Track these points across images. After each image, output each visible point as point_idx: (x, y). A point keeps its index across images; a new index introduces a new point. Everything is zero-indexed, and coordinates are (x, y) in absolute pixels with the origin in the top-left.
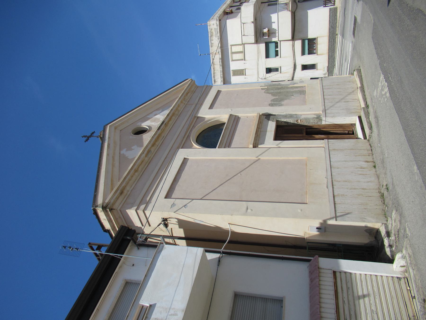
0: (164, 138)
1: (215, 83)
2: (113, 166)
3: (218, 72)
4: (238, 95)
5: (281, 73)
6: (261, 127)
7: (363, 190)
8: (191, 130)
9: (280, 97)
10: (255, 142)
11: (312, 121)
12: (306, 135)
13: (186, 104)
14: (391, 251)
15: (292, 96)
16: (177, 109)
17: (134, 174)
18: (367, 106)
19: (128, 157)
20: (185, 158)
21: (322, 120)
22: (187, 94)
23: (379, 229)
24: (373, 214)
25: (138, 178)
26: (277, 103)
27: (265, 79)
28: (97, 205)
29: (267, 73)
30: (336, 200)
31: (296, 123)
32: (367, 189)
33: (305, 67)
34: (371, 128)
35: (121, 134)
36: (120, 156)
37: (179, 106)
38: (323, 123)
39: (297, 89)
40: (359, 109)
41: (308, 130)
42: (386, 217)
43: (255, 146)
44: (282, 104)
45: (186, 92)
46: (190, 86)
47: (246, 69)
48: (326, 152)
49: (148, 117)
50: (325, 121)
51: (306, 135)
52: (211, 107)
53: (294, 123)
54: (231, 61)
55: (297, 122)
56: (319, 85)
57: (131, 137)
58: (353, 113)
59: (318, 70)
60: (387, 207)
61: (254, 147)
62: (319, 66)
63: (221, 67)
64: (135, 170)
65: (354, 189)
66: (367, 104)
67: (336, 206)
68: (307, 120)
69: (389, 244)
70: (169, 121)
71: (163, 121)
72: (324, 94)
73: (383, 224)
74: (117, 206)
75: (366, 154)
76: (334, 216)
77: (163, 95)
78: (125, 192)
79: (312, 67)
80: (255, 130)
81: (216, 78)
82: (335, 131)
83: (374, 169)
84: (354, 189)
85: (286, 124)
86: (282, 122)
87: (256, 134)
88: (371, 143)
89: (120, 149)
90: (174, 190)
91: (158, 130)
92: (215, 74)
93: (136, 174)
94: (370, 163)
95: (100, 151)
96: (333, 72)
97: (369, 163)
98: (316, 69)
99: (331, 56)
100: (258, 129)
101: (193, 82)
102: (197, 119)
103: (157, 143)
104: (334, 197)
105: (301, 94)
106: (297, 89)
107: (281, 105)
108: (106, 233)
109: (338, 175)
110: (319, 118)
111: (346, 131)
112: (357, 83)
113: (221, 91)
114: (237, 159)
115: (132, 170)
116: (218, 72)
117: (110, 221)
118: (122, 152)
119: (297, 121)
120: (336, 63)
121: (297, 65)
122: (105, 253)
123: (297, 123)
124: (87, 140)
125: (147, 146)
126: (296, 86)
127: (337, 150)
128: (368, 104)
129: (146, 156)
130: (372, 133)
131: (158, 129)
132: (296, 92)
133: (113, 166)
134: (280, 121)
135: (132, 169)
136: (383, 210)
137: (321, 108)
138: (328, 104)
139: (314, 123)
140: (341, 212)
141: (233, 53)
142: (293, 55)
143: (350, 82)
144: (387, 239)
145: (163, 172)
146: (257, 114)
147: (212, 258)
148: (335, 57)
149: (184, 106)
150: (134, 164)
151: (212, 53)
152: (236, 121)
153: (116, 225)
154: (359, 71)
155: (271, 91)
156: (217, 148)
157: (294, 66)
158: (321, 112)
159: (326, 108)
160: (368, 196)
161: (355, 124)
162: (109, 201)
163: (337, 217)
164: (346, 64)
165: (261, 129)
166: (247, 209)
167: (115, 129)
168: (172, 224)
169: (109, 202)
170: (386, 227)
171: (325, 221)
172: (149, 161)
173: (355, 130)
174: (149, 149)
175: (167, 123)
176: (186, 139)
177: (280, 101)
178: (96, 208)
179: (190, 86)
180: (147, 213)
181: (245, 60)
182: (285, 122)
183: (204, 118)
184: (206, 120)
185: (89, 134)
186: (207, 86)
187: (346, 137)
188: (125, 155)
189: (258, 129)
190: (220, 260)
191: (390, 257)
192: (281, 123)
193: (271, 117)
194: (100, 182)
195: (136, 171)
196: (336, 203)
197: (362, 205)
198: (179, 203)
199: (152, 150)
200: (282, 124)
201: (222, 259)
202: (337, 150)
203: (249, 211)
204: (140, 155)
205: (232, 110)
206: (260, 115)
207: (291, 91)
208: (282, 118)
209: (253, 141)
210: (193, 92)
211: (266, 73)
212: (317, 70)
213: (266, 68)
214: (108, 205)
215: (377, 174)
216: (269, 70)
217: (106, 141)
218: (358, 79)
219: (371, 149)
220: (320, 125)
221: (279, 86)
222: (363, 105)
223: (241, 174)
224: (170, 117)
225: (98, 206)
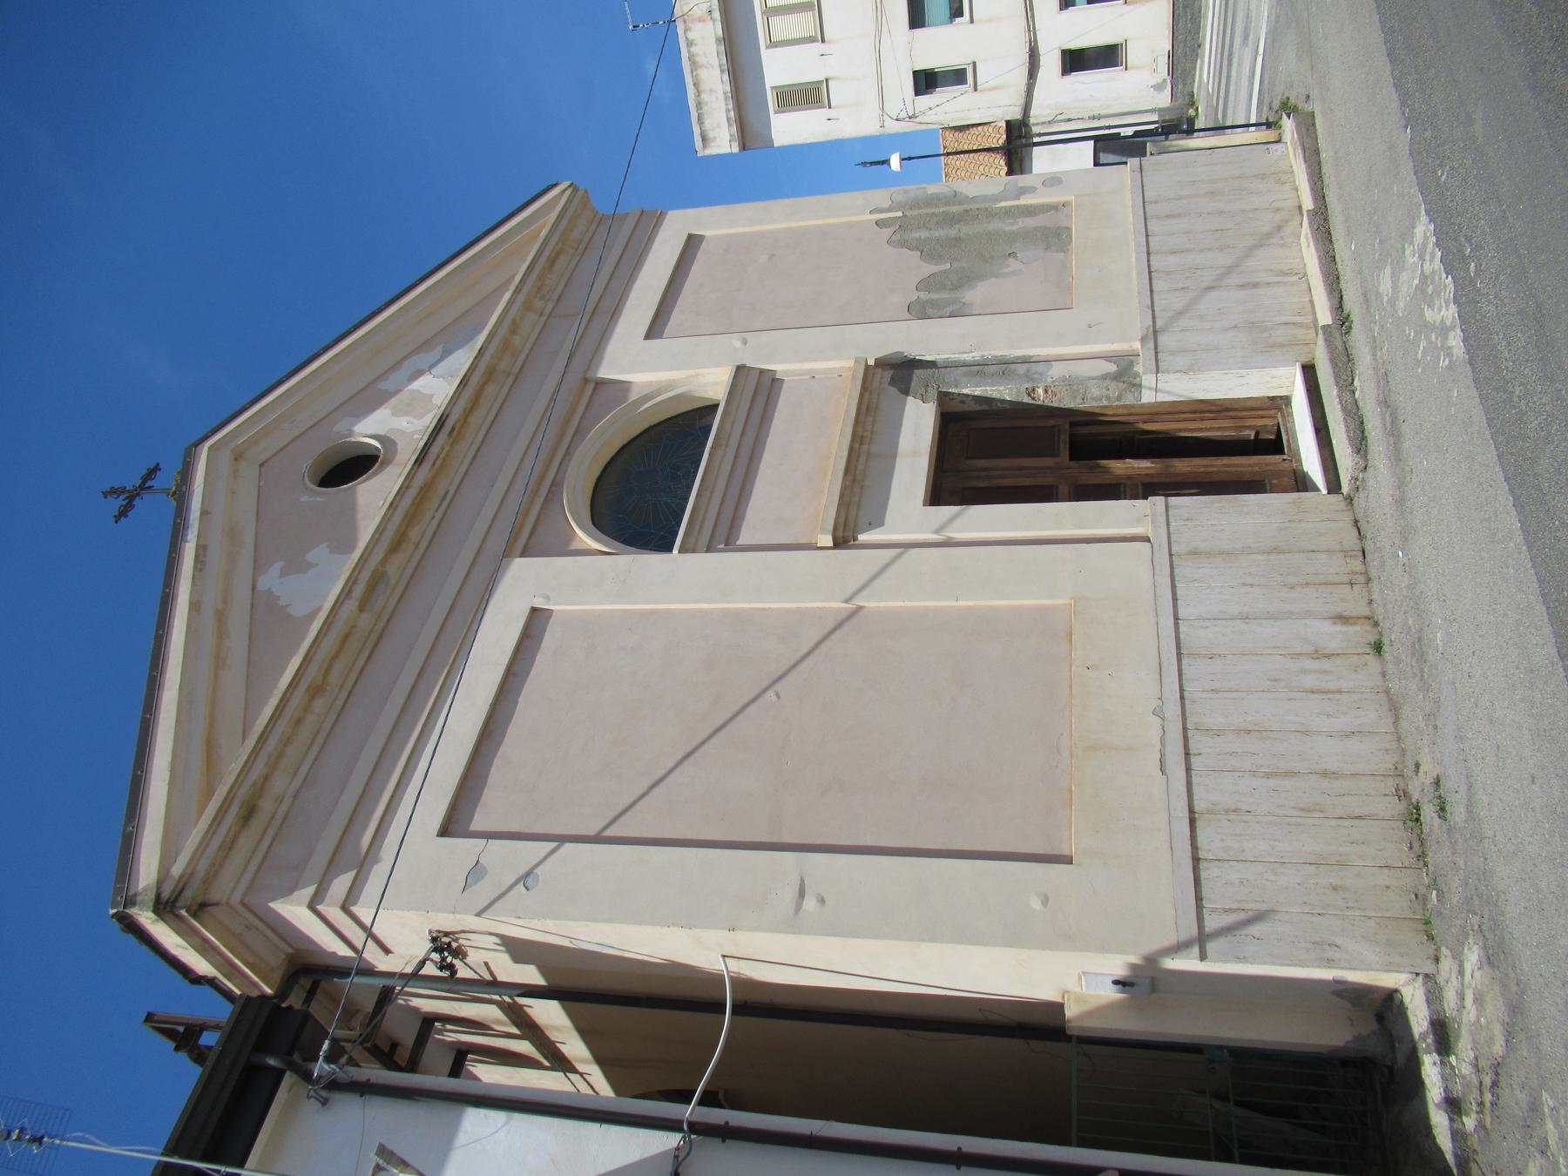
0: (445, 503)
1: (704, 146)
2: (219, 661)
3: (717, 98)
4: (773, 255)
5: (976, 89)
6: (872, 433)
7: (1325, 784)
8: (568, 454)
9: (955, 265)
10: (842, 520)
11: (1095, 391)
12: (1071, 459)
13: (547, 312)
14: (1458, 1135)
15: (1011, 260)
16: (506, 346)
17: (307, 708)
18: (1343, 320)
19: (288, 610)
20: (534, 610)
21: (1140, 386)
22: (552, 261)
23: (1396, 991)
24: (1370, 918)
25: (327, 725)
26: (945, 295)
27: (910, 118)
28: (131, 892)
29: (918, 92)
30: (1202, 839)
31: (1026, 400)
32: (1343, 776)
33: (1075, 61)
34: (1360, 444)
35: (261, 484)
36: (252, 605)
37: (514, 328)
38: (1147, 397)
39: (1031, 222)
40: (1308, 328)
41: (1082, 430)
42: (1431, 938)
43: (843, 537)
44: (964, 303)
45: (547, 253)
46: (564, 223)
47: (830, 83)
48: (1157, 567)
49: (383, 385)
50: (1156, 390)
51: (1071, 459)
52: (655, 330)
53: (1020, 400)
54: (767, 48)
55: (1029, 395)
56: (1128, 200)
57: (305, 499)
58: (1281, 345)
59: (1132, 68)
60: (1438, 892)
61: (841, 541)
62: (1133, 55)
63: (726, 77)
64: (310, 686)
65: (1288, 774)
66: (1341, 307)
67: (1203, 875)
68: (1075, 387)
69: (1445, 1091)
70: (468, 413)
71: (443, 414)
72: (1151, 244)
73: (1417, 974)
74: (226, 889)
75: (1336, 579)
76: (1194, 932)
77: (448, 275)
78: (266, 804)
79: (1107, 56)
80: (845, 454)
81: (708, 123)
82: (1200, 430)
83: (1373, 662)
84: (1288, 774)
85: (985, 407)
86: (965, 398)
87: (847, 471)
88: (1360, 516)
89: (257, 568)
90: (482, 789)
91: (419, 466)
92: (705, 108)
93: (319, 704)
94: (1357, 628)
95: (164, 592)
96: (1194, 75)
97: (1351, 629)
98: (1122, 65)
99: (1185, 7)
100: (857, 446)
101: (580, 194)
102: (595, 389)
103: (414, 534)
104: (1192, 821)
105: (1047, 248)
106: (1031, 222)
107: (959, 312)
108: (201, 987)
109: (1210, 695)
110: (1124, 372)
111: (1247, 432)
112: (1297, 183)
113: (701, 238)
114: (764, 609)
115: (295, 687)
116: (717, 98)
117: (205, 949)
118: (264, 583)
119: (1031, 392)
120: (1204, 36)
121: (1041, 53)
122: (163, 1154)
123: (1033, 402)
124: (123, 513)
125: (364, 558)
126: (1026, 206)
127: (1210, 554)
128: (1347, 307)
129: (361, 609)
130: (1365, 468)
131: (419, 461)
132: (1029, 237)
133: (219, 661)
134: (955, 396)
135: (297, 684)
136: (1416, 896)
137: (1139, 322)
138: (1168, 301)
139: (1108, 398)
140: (1226, 911)
141: (770, 12)
142: (1024, 10)
143: (1263, 177)
144: (1435, 1064)
145: (432, 700)
146: (853, 362)
147: (645, 1156)
148: (1200, 12)
149: (538, 328)
150: (304, 659)
151: (686, 17)
152: (761, 399)
153: (237, 961)
154: (1307, 126)
155: (916, 235)
156: (675, 551)
157: (1030, 56)
158: (1137, 345)
159: (1159, 324)
160: (1349, 818)
161: (1287, 400)
162: (185, 870)
163: (1208, 936)
164: (1248, 52)
165: (869, 444)
166: (802, 893)
167: (236, 459)
168: (482, 950)
169: (189, 871)
170: (1433, 996)
171: (1151, 960)
172: (379, 628)
173: (1286, 431)
174: (375, 571)
175: (458, 426)
176: (545, 501)
177: (955, 288)
178: (127, 911)
179: (564, 223)
180: (364, 912)
181: (823, 41)
182: (978, 399)
183: (625, 386)
184: (634, 396)
185: (133, 481)
186: (642, 212)
187: (1250, 465)
188: (278, 598)
189: (857, 446)
190: (679, 1171)
191: (1451, 1165)
192: (963, 402)
193: (918, 374)
194: (155, 761)
195: (316, 691)
196: (1202, 855)
197: (1322, 868)
198: (506, 858)
199: (393, 569)
200: (966, 408)
201: (687, 1161)
202: (1210, 554)
203: (810, 904)
204: (335, 605)
205: (745, 342)
206: (867, 367)
207: (1007, 229)
208: (965, 379)
209: (833, 513)
210: (580, 250)
211: (916, 94)
212: (1126, 69)
213: (915, 73)
214: (185, 885)
215: (1387, 692)
216: (926, 81)
217: (190, 532)
218: (1303, 166)
219: (1358, 547)
220: (1132, 406)
221: (954, 205)
222: (1325, 317)
223: (778, 695)
224: (471, 390)
225: (139, 899)
